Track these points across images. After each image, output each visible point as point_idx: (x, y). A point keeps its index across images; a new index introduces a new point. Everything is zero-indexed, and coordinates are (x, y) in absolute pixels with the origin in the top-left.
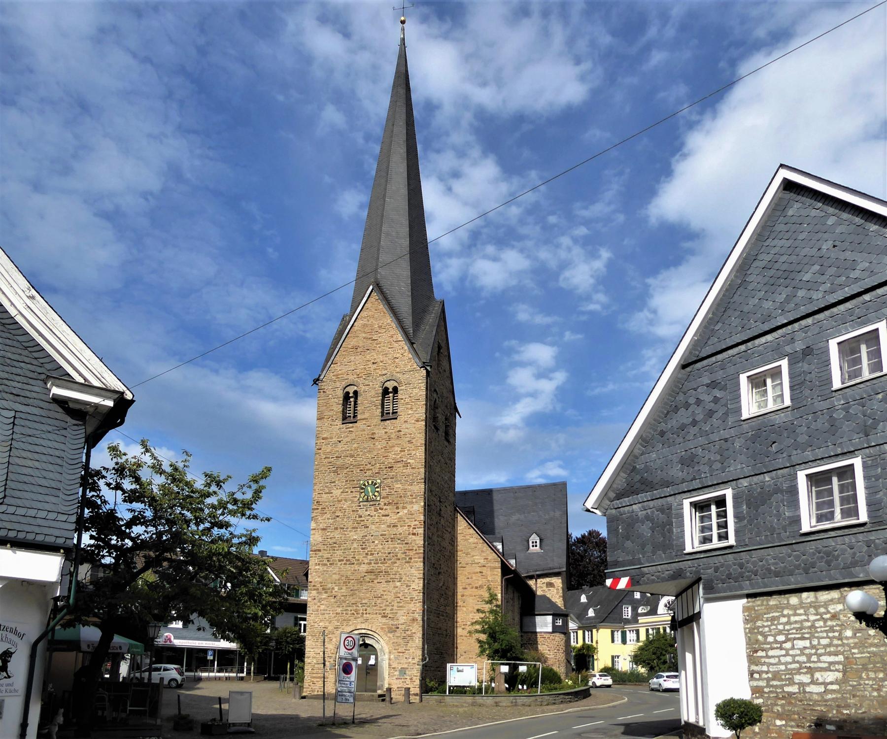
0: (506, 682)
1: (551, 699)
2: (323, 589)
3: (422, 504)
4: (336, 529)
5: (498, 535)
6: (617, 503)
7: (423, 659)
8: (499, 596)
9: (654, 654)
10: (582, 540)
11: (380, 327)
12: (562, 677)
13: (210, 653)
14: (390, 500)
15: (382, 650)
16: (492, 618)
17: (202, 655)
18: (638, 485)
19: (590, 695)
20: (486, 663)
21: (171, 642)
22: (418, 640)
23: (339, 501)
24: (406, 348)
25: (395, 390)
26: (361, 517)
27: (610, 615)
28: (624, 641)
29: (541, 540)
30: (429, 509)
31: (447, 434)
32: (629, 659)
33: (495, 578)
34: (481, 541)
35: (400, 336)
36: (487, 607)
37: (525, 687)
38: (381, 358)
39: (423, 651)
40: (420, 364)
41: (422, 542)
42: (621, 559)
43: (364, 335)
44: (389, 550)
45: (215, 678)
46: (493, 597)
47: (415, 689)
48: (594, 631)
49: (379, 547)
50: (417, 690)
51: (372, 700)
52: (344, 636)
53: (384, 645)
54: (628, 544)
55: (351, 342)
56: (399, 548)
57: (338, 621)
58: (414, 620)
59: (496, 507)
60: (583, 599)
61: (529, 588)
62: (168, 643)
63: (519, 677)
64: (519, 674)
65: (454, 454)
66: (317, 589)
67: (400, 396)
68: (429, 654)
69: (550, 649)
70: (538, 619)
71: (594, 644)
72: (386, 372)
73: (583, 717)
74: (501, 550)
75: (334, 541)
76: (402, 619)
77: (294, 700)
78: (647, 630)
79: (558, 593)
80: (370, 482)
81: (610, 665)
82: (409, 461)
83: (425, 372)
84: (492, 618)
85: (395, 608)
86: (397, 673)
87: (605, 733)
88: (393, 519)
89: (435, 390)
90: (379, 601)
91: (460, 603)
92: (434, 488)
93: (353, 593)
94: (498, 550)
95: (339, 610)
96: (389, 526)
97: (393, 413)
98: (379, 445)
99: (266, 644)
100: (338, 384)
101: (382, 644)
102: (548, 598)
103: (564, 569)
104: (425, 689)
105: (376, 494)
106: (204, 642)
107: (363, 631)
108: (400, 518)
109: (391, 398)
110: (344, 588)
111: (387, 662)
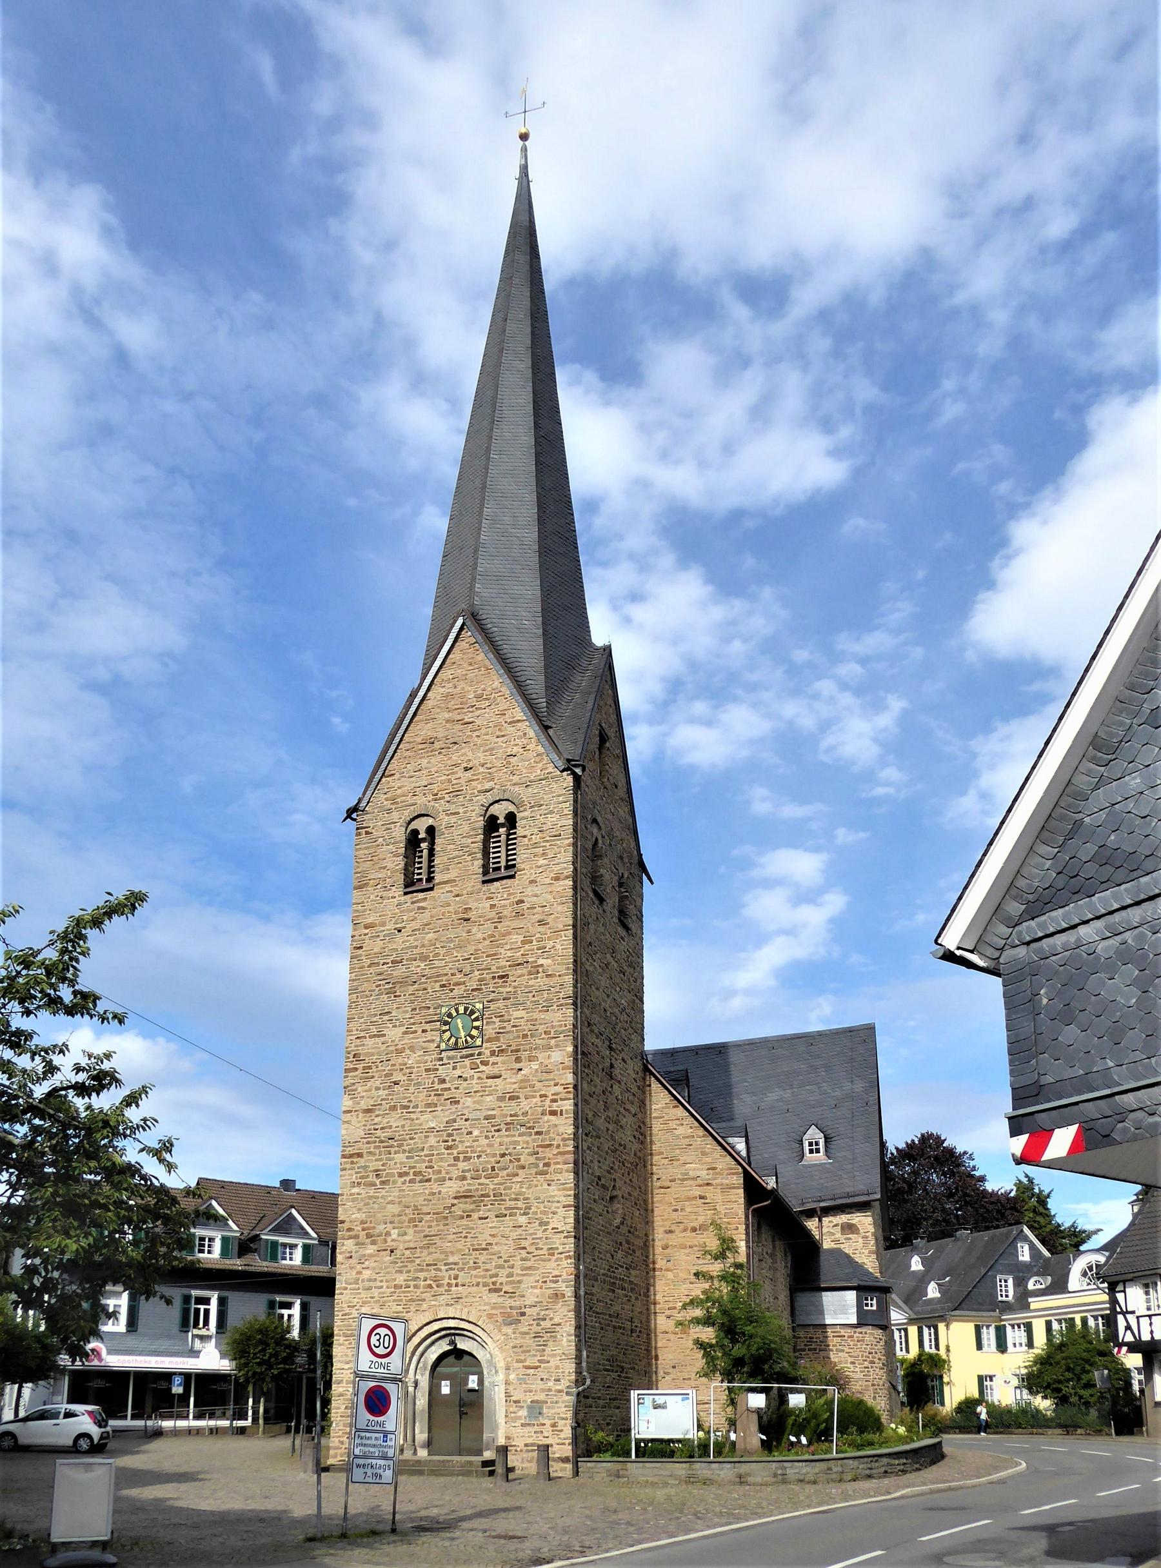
0: (762, 1431)
1: (862, 1466)
2: (368, 1236)
3: (570, 1049)
4: (393, 1108)
5: (739, 1123)
6: (1032, 928)
7: (579, 1381)
8: (742, 1245)
9: (1068, 1369)
10: (910, 1153)
11: (479, 697)
12: (884, 1419)
13: (178, 1380)
14: (502, 1043)
15: (491, 1363)
16: (725, 1289)
17: (163, 1385)
18: (1090, 870)
19: (943, 1456)
20: (717, 1387)
22: (566, 1340)
23: (399, 1052)
24: (532, 734)
25: (511, 819)
26: (443, 1081)
27: (971, 1298)
28: (1002, 1347)
29: (827, 1139)
30: (583, 1058)
31: (622, 913)
32: (1015, 1382)
33: (733, 1208)
34: (701, 1132)
35: (519, 712)
36: (716, 1268)
37: (804, 1440)
38: (481, 756)
39: (579, 1364)
40: (561, 764)
41: (571, 1130)
42: (1049, 1079)
43: (447, 715)
44: (503, 1149)
45: (189, 1431)
46: (727, 1246)
47: (562, 1447)
48: (941, 1327)
50: (567, 1451)
51: (468, 1473)
52: (368, 1324)
53: (496, 1352)
54: (1070, 1034)
55: (421, 731)
56: (523, 1144)
57: (398, 1302)
58: (557, 1296)
59: (736, 1076)
60: (916, 1264)
61: (807, 1234)
63: (790, 1421)
64: (792, 1412)
65: (640, 956)
66: (356, 1237)
67: (520, 831)
68: (594, 1369)
69: (854, 1353)
70: (828, 1298)
71: (942, 1352)
72: (491, 784)
73: (942, 1510)
74: (744, 1153)
75: (389, 1134)
76: (532, 1295)
77: (302, 1475)
78: (1049, 1324)
79: (865, 1244)
80: (461, 1009)
81: (976, 1395)
83: (570, 779)
84: (725, 1289)
85: (516, 1271)
86: (523, 1413)
87: (1001, 1555)
88: (510, 1082)
89: (595, 821)
90: (482, 1258)
91: (660, 1263)
92: (596, 1019)
93: (429, 1241)
94: (738, 1153)
95: (400, 1279)
96: (501, 1099)
97: (507, 867)
98: (478, 933)
99: (289, 1359)
100: (395, 816)
101: (492, 1351)
102: (848, 1256)
103: (878, 1196)
104: (585, 1448)
105: (474, 1032)
106: (148, 1358)
108: (525, 1080)
109: (503, 837)
110: (411, 1231)
111: (503, 1388)
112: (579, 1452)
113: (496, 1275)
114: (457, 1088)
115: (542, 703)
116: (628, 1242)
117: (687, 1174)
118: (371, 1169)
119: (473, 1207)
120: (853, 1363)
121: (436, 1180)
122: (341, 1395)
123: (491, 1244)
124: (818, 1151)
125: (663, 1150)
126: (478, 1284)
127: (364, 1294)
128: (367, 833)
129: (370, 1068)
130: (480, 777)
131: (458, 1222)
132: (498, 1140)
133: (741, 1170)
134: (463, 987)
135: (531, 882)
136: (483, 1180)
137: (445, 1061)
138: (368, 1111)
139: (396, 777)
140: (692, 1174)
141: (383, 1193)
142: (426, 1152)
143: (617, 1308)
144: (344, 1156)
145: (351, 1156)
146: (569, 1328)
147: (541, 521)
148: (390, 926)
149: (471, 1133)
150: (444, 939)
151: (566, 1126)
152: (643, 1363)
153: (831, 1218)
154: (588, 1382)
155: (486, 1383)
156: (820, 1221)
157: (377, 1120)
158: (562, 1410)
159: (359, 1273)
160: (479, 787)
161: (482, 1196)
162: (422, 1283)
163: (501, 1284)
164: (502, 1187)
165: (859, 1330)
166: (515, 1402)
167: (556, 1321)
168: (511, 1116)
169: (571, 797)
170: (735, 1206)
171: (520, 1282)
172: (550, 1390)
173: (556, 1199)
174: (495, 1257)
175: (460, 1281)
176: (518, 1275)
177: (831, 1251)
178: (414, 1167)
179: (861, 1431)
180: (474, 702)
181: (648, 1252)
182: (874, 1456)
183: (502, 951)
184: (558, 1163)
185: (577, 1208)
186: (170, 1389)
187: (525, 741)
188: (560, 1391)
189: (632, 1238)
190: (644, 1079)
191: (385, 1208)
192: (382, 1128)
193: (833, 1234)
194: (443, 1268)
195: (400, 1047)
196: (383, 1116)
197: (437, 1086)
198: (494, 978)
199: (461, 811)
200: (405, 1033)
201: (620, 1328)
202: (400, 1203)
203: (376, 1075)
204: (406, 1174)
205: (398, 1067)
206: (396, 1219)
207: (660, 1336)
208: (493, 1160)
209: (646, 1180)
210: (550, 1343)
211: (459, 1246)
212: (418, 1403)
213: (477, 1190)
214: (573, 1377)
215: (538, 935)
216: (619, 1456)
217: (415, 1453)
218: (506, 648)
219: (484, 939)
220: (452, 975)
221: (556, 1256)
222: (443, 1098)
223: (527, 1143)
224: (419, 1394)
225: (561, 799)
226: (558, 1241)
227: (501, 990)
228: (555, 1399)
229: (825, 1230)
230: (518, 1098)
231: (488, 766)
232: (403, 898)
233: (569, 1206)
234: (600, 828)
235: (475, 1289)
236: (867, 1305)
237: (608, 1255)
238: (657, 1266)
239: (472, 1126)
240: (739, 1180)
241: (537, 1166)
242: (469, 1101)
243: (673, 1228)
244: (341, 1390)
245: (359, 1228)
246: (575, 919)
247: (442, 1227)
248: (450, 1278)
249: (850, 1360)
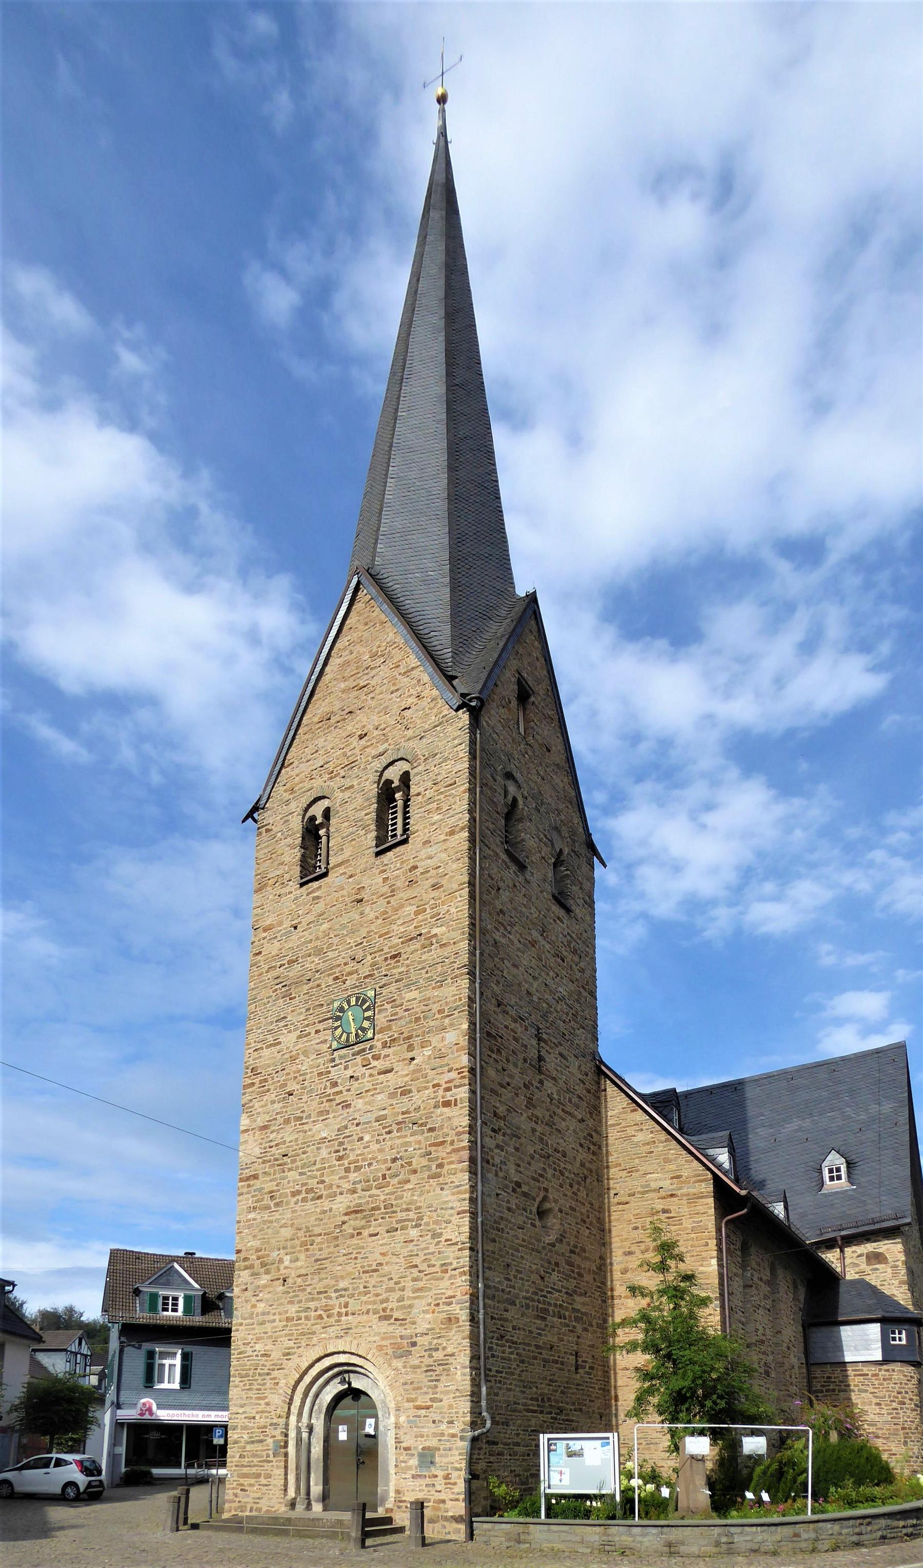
1: (847, 1532)
2: (263, 1265)
3: (465, 1026)
4: (287, 1121)
21: (151, 1413)
22: (460, 1375)
24: (426, 678)
26: (335, 1084)
29: (849, 1165)
34: (663, 1136)
38: (375, 719)
41: (465, 1121)
49: (373, 1149)
50: (460, 1508)
56: (413, 1143)
58: (450, 1320)
59: (752, 1111)
62: (147, 1416)
66: (251, 1267)
67: (414, 790)
70: (847, 1333)
74: (727, 1165)
75: (283, 1151)
76: (424, 1320)
79: (895, 1275)
82: (435, 931)
85: (408, 1293)
86: (414, 1462)
90: (373, 1281)
95: (292, 1310)
96: (392, 1095)
100: (293, 806)
102: (874, 1289)
104: (482, 1503)
105: (366, 1024)
106: (213, 1413)
107: (342, 1359)
110: (302, 1256)
112: (478, 1510)
113: (387, 1300)
114: (349, 1090)
115: (447, 654)
116: (570, 1264)
117: (648, 1186)
118: (266, 1190)
119: (363, 1222)
120: (878, 1404)
121: (329, 1196)
122: (236, 1442)
123: (381, 1264)
124: (839, 1178)
125: (620, 1160)
126: (368, 1312)
127: (258, 1330)
128: (268, 831)
129: (266, 1080)
130: (374, 741)
131: (349, 1242)
132: (389, 1143)
133: (710, 1176)
134: (355, 976)
135: (425, 843)
136: (374, 1191)
137: (337, 1062)
138: (265, 1128)
139: (294, 765)
140: (654, 1185)
141: (277, 1216)
142: (318, 1166)
143: (549, 1338)
144: (241, 1180)
145: (248, 1179)
146: (464, 1358)
147: (452, 468)
148: (287, 924)
149: (361, 1139)
150: (337, 926)
151: (460, 1118)
152: (598, 1403)
153: (854, 1248)
154: (488, 1424)
155: (381, 1428)
156: (842, 1251)
157: (272, 1136)
158: (455, 1459)
159: (254, 1306)
160: (374, 752)
161: (373, 1209)
162: (313, 1314)
163: (392, 1309)
164: (393, 1197)
165: (885, 1367)
166: (406, 1449)
167: (450, 1350)
168: (403, 1113)
169: (467, 738)
170: (704, 1218)
171: (411, 1306)
172: (442, 1434)
173: (450, 1205)
174: (385, 1279)
175: (350, 1309)
176: (409, 1298)
177: (853, 1282)
178: (306, 1184)
179: (859, 1483)
180: (369, 662)
181: (605, 1277)
182: (864, 1517)
183: (395, 927)
184: (452, 1163)
185: (473, 1215)
186: (212, 1441)
187: (419, 689)
188: (453, 1436)
189: (576, 1259)
190: (598, 1083)
191: (278, 1233)
192: (277, 1145)
193: (857, 1265)
194: (334, 1295)
195: (294, 1053)
196: (278, 1131)
197: (329, 1091)
198: (386, 959)
199: (355, 783)
200: (300, 1037)
201: (556, 1362)
202: (292, 1225)
203: (272, 1087)
204: (299, 1192)
205: (292, 1075)
206: (289, 1244)
207: (620, 1373)
208: (383, 1167)
209: (601, 1196)
210: (443, 1378)
211: (349, 1268)
212: (313, 1450)
213: (368, 1203)
214: (468, 1419)
215: (432, 902)
216: (527, 1515)
217: (309, 1506)
218: (409, 604)
219: (377, 918)
220: (345, 964)
221: (450, 1273)
222: (334, 1103)
223: (419, 1142)
224: (313, 1441)
225: (456, 742)
226: (452, 1255)
227: (394, 971)
228: (448, 1445)
229: (848, 1261)
230: (410, 1091)
231: (382, 727)
232: (298, 892)
233: (464, 1212)
234: (519, 787)
235: (365, 1317)
236: (894, 1339)
237: (534, 1277)
238: (616, 1293)
239: (364, 1131)
240: (708, 1187)
241: (429, 1168)
242: (359, 1103)
243: (634, 1248)
244: (236, 1436)
245: (254, 1257)
246: (472, 875)
247: (332, 1249)
248: (340, 1307)
249: (875, 1401)
